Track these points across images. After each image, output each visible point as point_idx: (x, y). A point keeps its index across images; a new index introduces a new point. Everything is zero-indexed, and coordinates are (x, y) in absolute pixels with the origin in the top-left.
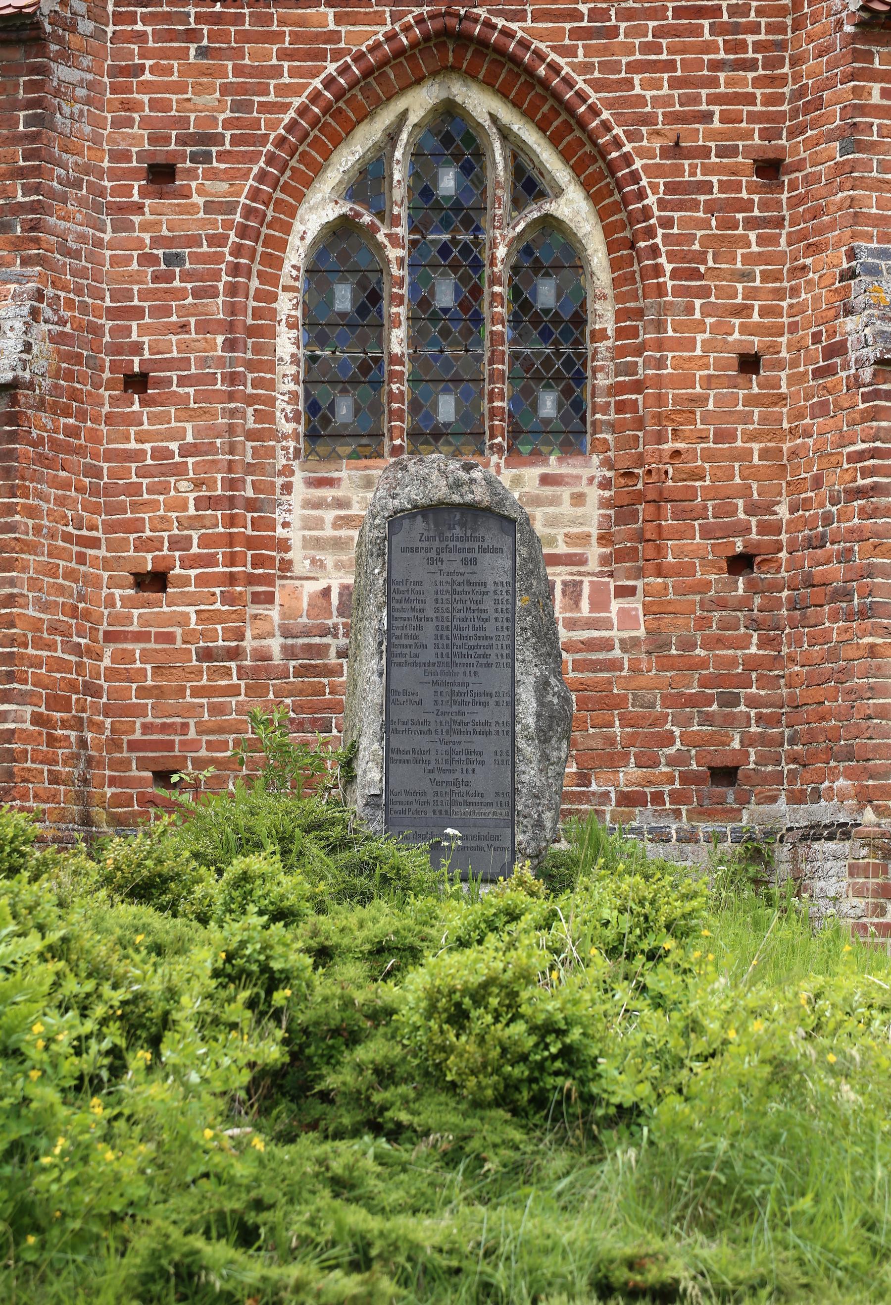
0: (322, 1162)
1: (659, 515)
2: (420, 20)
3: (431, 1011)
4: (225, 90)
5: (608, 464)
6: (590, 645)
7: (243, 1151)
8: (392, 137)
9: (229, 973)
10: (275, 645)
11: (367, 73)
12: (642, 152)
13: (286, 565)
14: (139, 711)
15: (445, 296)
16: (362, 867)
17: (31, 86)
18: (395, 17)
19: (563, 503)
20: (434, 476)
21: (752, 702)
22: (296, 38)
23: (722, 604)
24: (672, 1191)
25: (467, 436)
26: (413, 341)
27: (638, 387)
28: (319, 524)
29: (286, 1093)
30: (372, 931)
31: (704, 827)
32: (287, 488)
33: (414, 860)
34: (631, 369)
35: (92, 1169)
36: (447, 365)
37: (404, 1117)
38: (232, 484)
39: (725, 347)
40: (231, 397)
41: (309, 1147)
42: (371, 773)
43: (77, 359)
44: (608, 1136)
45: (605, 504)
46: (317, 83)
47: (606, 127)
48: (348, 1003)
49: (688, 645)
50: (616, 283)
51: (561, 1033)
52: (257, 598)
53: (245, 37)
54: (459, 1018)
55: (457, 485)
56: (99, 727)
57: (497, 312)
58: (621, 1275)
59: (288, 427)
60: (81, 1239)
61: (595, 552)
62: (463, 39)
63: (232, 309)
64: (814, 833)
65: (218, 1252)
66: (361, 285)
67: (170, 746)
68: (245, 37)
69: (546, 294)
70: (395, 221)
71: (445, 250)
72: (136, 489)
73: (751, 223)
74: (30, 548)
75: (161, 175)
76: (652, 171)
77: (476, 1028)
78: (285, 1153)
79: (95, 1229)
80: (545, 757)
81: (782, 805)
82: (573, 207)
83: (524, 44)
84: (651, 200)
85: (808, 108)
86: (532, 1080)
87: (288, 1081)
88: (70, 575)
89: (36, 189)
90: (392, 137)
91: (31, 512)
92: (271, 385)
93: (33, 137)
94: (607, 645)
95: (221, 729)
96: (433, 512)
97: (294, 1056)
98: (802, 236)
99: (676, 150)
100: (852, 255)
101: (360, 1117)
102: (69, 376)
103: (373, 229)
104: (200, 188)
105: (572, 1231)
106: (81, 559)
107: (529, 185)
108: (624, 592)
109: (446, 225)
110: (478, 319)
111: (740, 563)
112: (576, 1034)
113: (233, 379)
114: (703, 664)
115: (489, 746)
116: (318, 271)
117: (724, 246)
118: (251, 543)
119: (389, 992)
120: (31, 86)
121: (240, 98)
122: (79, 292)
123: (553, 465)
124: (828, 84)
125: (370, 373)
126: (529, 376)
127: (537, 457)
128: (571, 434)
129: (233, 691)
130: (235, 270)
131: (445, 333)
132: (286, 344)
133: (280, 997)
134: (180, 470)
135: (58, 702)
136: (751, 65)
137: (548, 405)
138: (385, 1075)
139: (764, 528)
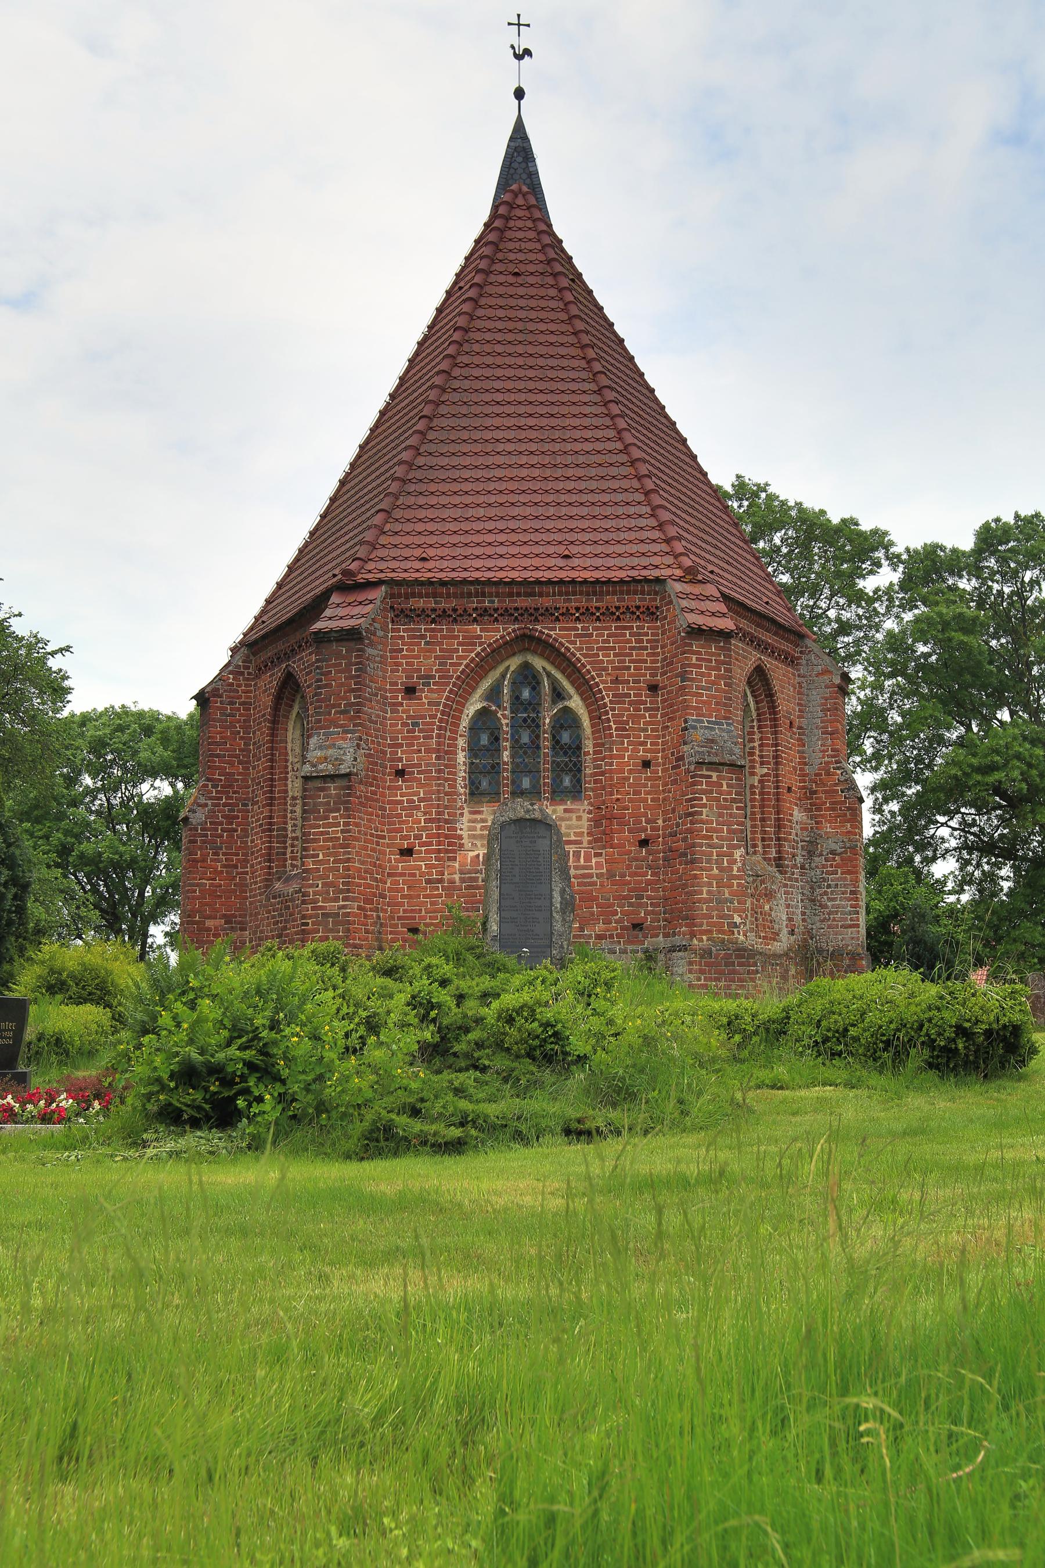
0: (451, 1082)
1: (611, 824)
2: (514, 631)
3: (499, 1019)
4: (436, 657)
5: (590, 804)
6: (584, 876)
7: (418, 1078)
8: (503, 676)
9: (414, 1002)
10: (457, 877)
11: (493, 651)
12: (602, 682)
13: (462, 845)
14: (402, 904)
15: (525, 739)
16: (489, 965)
17: (357, 657)
18: (504, 629)
19: (572, 820)
20: (521, 808)
21: (649, 898)
22: (464, 637)
23: (636, 859)
24: (598, 1090)
25: (534, 793)
26: (512, 756)
27: (602, 774)
28: (475, 829)
29: (435, 1054)
30: (482, 987)
31: (630, 947)
32: (462, 815)
33: (511, 961)
34: (599, 767)
35: (350, 1085)
36: (526, 766)
37: (487, 1063)
38: (438, 813)
39: (637, 757)
40: (439, 778)
41: (447, 1075)
42: (494, 927)
43: (376, 764)
44: (574, 1068)
45: (589, 820)
46: (473, 655)
47: (589, 672)
48: (465, 1016)
49: (623, 875)
50: (593, 733)
51: (553, 1026)
52: (449, 859)
53: (443, 637)
54: (510, 1021)
55: (528, 811)
56: (386, 911)
57: (546, 744)
58: (574, 1125)
59: (462, 791)
60: (344, 1115)
61: (586, 839)
62: (531, 638)
63: (438, 744)
64: (673, 949)
65: (403, 1120)
66: (492, 734)
67: (414, 918)
68: (443, 637)
69: (565, 737)
70: (505, 709)
71: (525, 720)
72: (400, 816)
73: (646, 709)
74: (357, 839)
75: (410, 691)
76: (606, 689)
77: (518, 1025)
78: (435, 1078)
79: (351, 1111)
80: (564, 920)
81: (661, 938)
82: (576, 703)
83: (556, 640)
84: (607, 700)
85: (668, 665)
86: (541, 1046)
87: (440, 1049)
88: (373, 850)
89: (359, 697)
90: (503, 676)
91: (357, 825)
92: (455, 774)
93: (358, 676)
94: (591, 876)
95: (435, 911)
96: (519, 821)
97: (442, 1038)
98: (667, 714)
99: (616, 681)
100: (686, 721)
101: (469, 1062)
102: (372, 771)
103: (496, 712)
104: (425, 696)
105: (553, 1108)
106: (378, 844)
107: (558, 695)
108: (597, 855)
109: (526, 710)
110: (538, 747)
111: (644, 843)
112: (559, 1026)
113: (439, 771)
114: (629, 883)
116: (474, 729)
118: (447, 837)
119: (484, 1011)
120: (357, 657)
121: (442, 660)
122: (377, 737)
123: (569, 805)
124: (675, 655)
125: (495, 769)
126: (559, 770)
127: (563, 802)
128: (576, 792)
129: (440, 896)
130: (440, 728)
131: (525, 753)
132: (461, 757)
133: (433, 1014)
134: (418, 808)
135: (367, 901)
136: (646, 648)
137: (567, 781)
138: (479, 1045)
139: (653, 829)
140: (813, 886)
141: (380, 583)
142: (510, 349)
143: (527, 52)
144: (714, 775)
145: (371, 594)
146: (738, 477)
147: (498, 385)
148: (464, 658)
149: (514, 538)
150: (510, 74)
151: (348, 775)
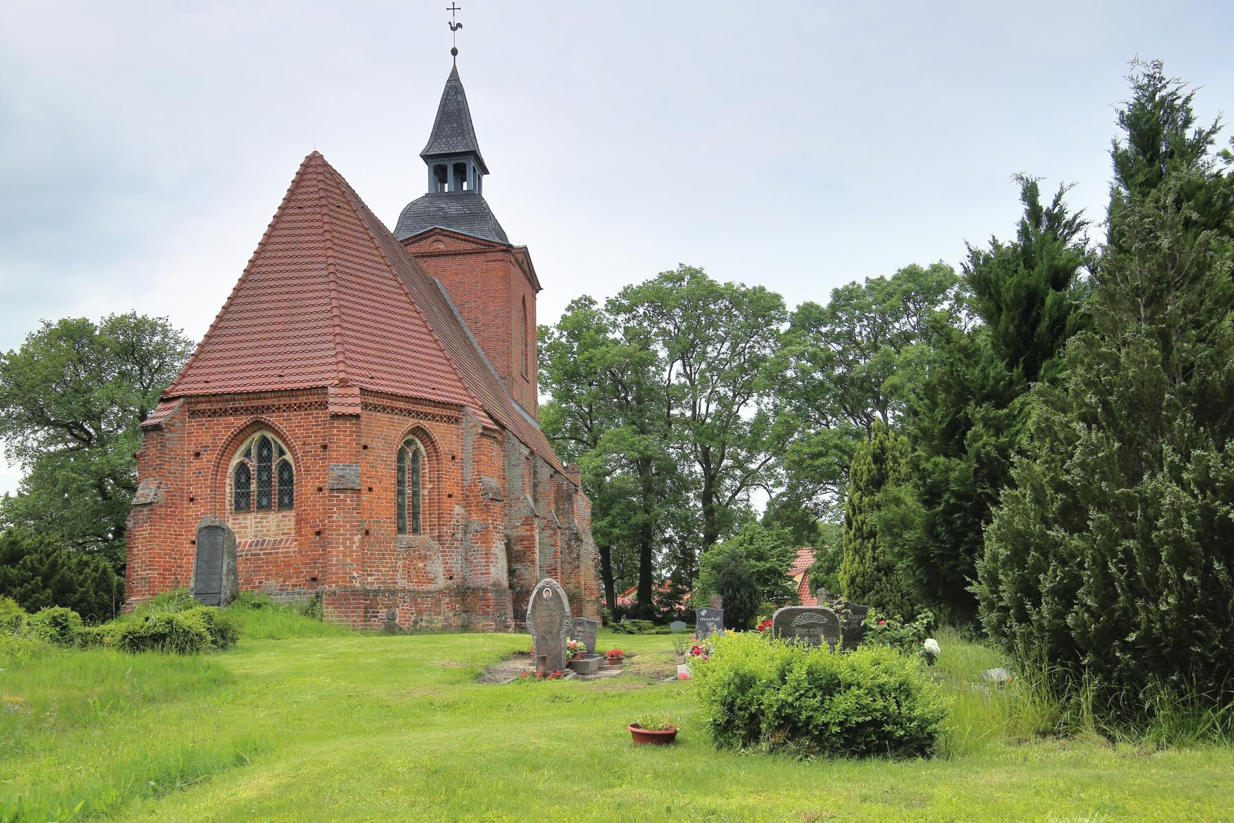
12: (297, 445)
15: (265, 478)
61: (293, 532)
75: (197, 455)
99: (304, 444)
104: (205, 457)
107: (282, 453)
111: (318, 533)
115: (216, 577)
117: (315, 464)
123: (285, 513)
125: (247, 495)
140: (467, 550)
141: (180, 397)
142: (285, 254)
143: (459, 25)
144: (342, 496)
145: (176, 404)
146: (1030, 193)
147: (273, 276)
148: (225, 435)
149: (257, 366)
150: (449, 39)
151: (150, 503)
